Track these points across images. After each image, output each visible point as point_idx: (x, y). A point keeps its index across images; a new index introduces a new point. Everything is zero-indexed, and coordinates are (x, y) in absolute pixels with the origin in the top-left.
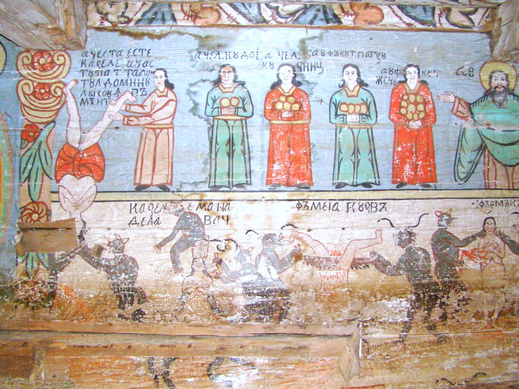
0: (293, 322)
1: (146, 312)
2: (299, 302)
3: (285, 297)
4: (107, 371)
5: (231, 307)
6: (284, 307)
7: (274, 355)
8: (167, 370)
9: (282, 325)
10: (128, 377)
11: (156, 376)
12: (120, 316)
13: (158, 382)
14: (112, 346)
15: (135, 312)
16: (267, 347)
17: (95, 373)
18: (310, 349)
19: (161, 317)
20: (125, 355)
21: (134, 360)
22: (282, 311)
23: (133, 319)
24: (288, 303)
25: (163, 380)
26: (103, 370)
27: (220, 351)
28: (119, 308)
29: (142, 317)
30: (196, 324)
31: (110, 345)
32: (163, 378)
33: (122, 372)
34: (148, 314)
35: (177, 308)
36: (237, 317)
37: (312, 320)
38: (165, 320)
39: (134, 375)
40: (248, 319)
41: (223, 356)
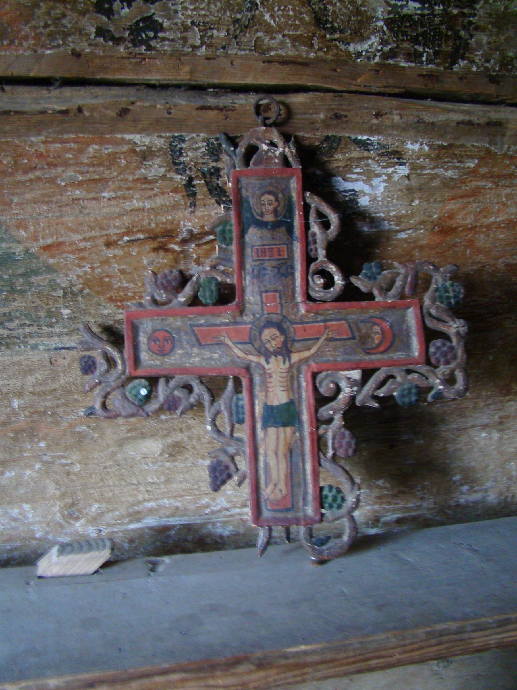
0: (478, 68)
1: (166, 25)
2: (492, 24)
3: (465, 11)
4: (70, 173)
5: (360, 22)
6: (463, 33)
7: (441, 137)
8: (214, 164)
9: (456, 73)
10: (122, 184)
11: (191, 179)
12: (101, 32)
13: (194, 194)
14: (80, 110)
15: (137, 23)
16: (428, 118)
17: (39, 179)
18: (506, 128)
19: (202, 37)
20: (112, 132)
21: (135, 143)
22: (458, 42)
23: (132, 41)
24: (470, 23)
25: (205, 189)
26: (60, 170)
27: (334, 122)
28: (98, 12)
29: (156, 37)
30: (280, 56)
31: (75, 108)
32: (207, 183)
33: (107, 172)
34: (170, 29)
35: (239, 16)
36: (371, 46)
37: (513, 67)
38: (210, 46)
39: (138, 180)
40: (393, 54)
41: (339, 135)
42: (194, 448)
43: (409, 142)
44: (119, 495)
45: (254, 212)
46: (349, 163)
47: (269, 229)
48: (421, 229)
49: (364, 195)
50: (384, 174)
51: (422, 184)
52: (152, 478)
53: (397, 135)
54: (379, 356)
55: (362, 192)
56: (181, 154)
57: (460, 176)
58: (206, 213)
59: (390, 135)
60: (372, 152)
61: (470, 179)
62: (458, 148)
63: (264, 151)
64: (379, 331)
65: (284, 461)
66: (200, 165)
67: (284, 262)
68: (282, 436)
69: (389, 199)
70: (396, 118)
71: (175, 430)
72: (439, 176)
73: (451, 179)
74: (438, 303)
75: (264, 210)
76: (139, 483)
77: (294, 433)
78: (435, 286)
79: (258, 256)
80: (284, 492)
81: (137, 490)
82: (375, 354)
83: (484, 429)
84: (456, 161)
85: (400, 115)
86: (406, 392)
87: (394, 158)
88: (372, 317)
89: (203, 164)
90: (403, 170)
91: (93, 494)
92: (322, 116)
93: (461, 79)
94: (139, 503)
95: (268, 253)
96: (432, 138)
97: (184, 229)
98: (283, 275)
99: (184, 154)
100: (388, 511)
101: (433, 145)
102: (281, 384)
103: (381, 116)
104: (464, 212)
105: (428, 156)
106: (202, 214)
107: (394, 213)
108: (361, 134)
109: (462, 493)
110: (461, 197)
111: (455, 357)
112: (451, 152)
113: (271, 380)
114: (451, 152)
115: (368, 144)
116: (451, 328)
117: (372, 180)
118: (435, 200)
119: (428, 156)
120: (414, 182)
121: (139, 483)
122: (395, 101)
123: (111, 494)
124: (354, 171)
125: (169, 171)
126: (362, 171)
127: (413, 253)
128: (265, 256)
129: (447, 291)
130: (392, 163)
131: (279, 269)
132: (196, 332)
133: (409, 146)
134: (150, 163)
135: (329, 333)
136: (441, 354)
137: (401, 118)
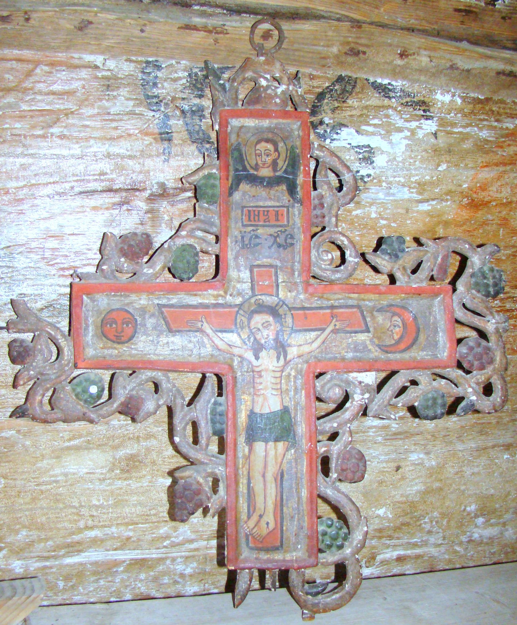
7: (478, 88)
9: (499, 11)
21: (96, 67)
27: (350, 59)
42: (154, 463)
43: (439, 92)
44: (55, 520)
45: (246, 163)
46: (365, 111)
47: (264, 186)
48: (447, 200)
49: (382, 154)
50: (407, 128)
51: (450, 145)
52: (99, 500)
53: (425, 82)
54: (398, 356)
55: (379, 149)
56: (155, 85)
57: (497, 138)
58: (183, 163)
59: (417, 81)
60: (393, 100)
61: (508, 142)
62: (497, 103)
63: (263, 86)
64: (401, 325)
65: (274, 485)
66: (180, 101)
67: (283, 229)
68: (272, 453)
69: (412, 161)
70: (424, 60)
71: (129, 439)
72: (472, 136)
73: (486, 141)
74: (474, 292)
75: (260, 162)
76: (81, 506)
77: (287, 450)
78: (471, 270)
79: (250, 220)
80: (272, 526)
81: (78, 514)
82: (395, 353)
83: (508, 449)
84: (492, 119)
85: (430, 57)
86: (430, 403)
87: (419, 109)
88: (391, 305)
89: (183, 99)
90: (430, 126)
91: (21, 517)
92: (335, 50)
93: (503, 18)
94: (80, 531)
95: (262, 218)
96: (466, 89)
97: (154, 182)
98: (279, 246)
99: (160, 86)
100: (388, 547)
101: (467, 97)
102: (275, 387)
103: (407, 56)
104: (499, 183)
105: (461, 110)
106: (178, 163)
107: (417, 178)
108: (381, 77)
109: (476, 526)
110: (497, 165)
111: (491, 361)
112: (487, 108)
113: (261, 380)
114: (487, 108)
115: (390, 90)
116: (489, 324)
117: (391, 135)
118: (466, 165)
119: (461, 110)
120: (442, 141)
121: (81, 506)
122: (426, 39)
123: (44, 519)
124: (371, 122)
125: (138, 105)
126: (380, 123)
127: (437, 229)
128: (259, 221)
129: (485, 278)
130: (416, 115)
131: (276, 238)
132: (166, 314)
133: (439, 96)
134: (115, 93)
135: (337, 323)
136: (474, 357)
137: (431, 61)
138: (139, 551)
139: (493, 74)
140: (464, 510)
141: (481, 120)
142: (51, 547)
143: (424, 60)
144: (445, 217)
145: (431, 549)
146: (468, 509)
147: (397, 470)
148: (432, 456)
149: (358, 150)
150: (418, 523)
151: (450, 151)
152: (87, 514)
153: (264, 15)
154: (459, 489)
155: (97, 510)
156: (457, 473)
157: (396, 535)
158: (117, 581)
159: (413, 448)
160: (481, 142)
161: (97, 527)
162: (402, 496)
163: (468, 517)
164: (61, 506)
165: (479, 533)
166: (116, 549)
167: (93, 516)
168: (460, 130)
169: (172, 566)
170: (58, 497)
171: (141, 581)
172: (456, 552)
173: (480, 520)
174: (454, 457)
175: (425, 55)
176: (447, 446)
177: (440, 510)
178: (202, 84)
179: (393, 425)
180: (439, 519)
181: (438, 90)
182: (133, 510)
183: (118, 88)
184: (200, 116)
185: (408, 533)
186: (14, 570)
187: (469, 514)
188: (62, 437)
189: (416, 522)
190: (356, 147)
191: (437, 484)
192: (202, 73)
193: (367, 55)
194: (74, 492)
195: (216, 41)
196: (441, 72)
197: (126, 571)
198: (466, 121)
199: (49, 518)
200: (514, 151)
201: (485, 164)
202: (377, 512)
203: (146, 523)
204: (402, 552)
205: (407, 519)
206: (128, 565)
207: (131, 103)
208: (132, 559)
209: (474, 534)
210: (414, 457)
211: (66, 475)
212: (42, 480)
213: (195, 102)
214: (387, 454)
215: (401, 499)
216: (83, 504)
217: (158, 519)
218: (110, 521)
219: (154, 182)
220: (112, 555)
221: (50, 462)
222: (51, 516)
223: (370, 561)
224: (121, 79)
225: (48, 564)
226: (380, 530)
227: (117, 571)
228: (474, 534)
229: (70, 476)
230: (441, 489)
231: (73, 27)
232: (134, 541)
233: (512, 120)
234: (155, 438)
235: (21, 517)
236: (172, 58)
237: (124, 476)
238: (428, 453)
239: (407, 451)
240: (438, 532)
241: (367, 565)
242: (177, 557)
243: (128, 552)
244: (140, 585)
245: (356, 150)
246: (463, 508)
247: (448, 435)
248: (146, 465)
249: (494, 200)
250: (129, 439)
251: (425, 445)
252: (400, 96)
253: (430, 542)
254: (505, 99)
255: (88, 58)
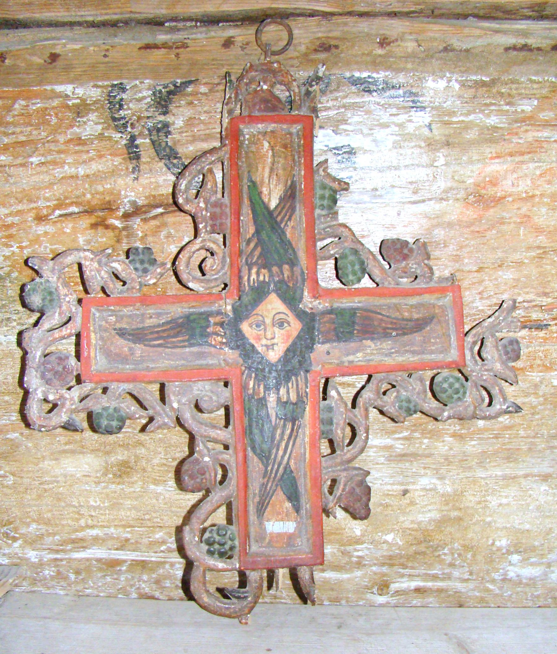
21: (67, 96)
42: (144, 470)
43: (431, 78)
44: (60, 517)
52: (96, 502)
53: (413, 70)
70: (411, 46)
73: (495, 129)
81: (78, 513)
84: (502, 103)
85: (417, 41)
89: (148, 118)
91: (30, 512)
94: (82, 529)
96: (463, 72)
99: (125, 107)
100: (402, 576)
103: (388, 44)
108: (359, 71)
109: (510, 564)
112: (494, 90)
120: (438, 132)
121: (80, 506)
134: (85, 119)
138: (139, 553)
139: (501, 50)
140: (493, 544)
141: (486, 105)
142: (59, 541)
143: (411, 46)
144: (447, 219)
145: (457, 584)
146: (498, 543)
147: (404, 495)
148: (447, 482)
149: (337, 152)
150: (437, 554)
151: (448, 144)
152: (86, 514)
153: (197, 21)
154: (483, 521)
155: (95, 511)
156: (479, 503)
157: (410, 564)
158: (122, 579)
159: (422, 471)
160: (488, 129)
161: (97, 526)
162: (412, 522)
163: (499, 553)
164: (63, 504)
165: (515, 572)
166: (117, 549)
167: (92, 516)
168: (461, 118)
169: (171, 571)
170: (60, 496)
171: (144, 582)
172: (488, 590)
173: (515, 558)
174: (474, 485)
175: (411, 40)
176: (465, 472)
177: (461, 542)
178: (166, 101)
179: (397, 446)
180: (462, 552)
181: (429, 76)
182: (128, 513)
183: (87, 114)
184: (165, 133)
185: (425, 563)
186: (30, 559)
187: (499, 549)
188: (59, 441)
189: (433, 552)
190: (334, 149)
191: (455, 514)
192: (166, 90)
193: (340, 49)
194: (73, 492)
195: (177, 55)
196: (432, 57)
197: (128, 571)
198: (468, 107)
199: (54, 514)
200: (534, 137)
201: (494, 155)
202: (384, 537)
203: (141, 527)
204: (421, 584)
205: (422, 548)
206: (130, 564)
207: (100, 127)
208: (133, 560)
209: (508, 573)
210: (424, 482)
211: (65, 476)
212: (44, 479)
213: (161, 119)
214: (392, 477)
215: (412, 526)
216: (82, 504)
217: (153, 524)
218: (108, 521)
219: (126, 200)
220: (114, 554)
221: (50, 463)
222: (55, 513)
223: (382, 589)
224: (90, 105)
225: (59, 556)
226: (391, 557)
227: (120, 570)
228: (508, 573)
229: (68, 478)
230: (460, 519)
231: (43, 61)
232: (132, 543)
233: (530, 101)
234: (143, 446)
235: (30, 512)
236: (136, 79)
237: (118, 480)
238: (442, 478)
239: (417, 475)
240: (463, 566)
241: (380, 592)
242: (175, 563)
243: (128, 552)
244: (143, 585)
245: (334, 151)
246: (490, 542)
247: (466, 460)
248: (136, 471)
249: (510, 196)
250: (120, 445)
251: (437, 470)
252: (383, 88)
253: (454, 575)
254: (517, 78)
255: (59, 88)
